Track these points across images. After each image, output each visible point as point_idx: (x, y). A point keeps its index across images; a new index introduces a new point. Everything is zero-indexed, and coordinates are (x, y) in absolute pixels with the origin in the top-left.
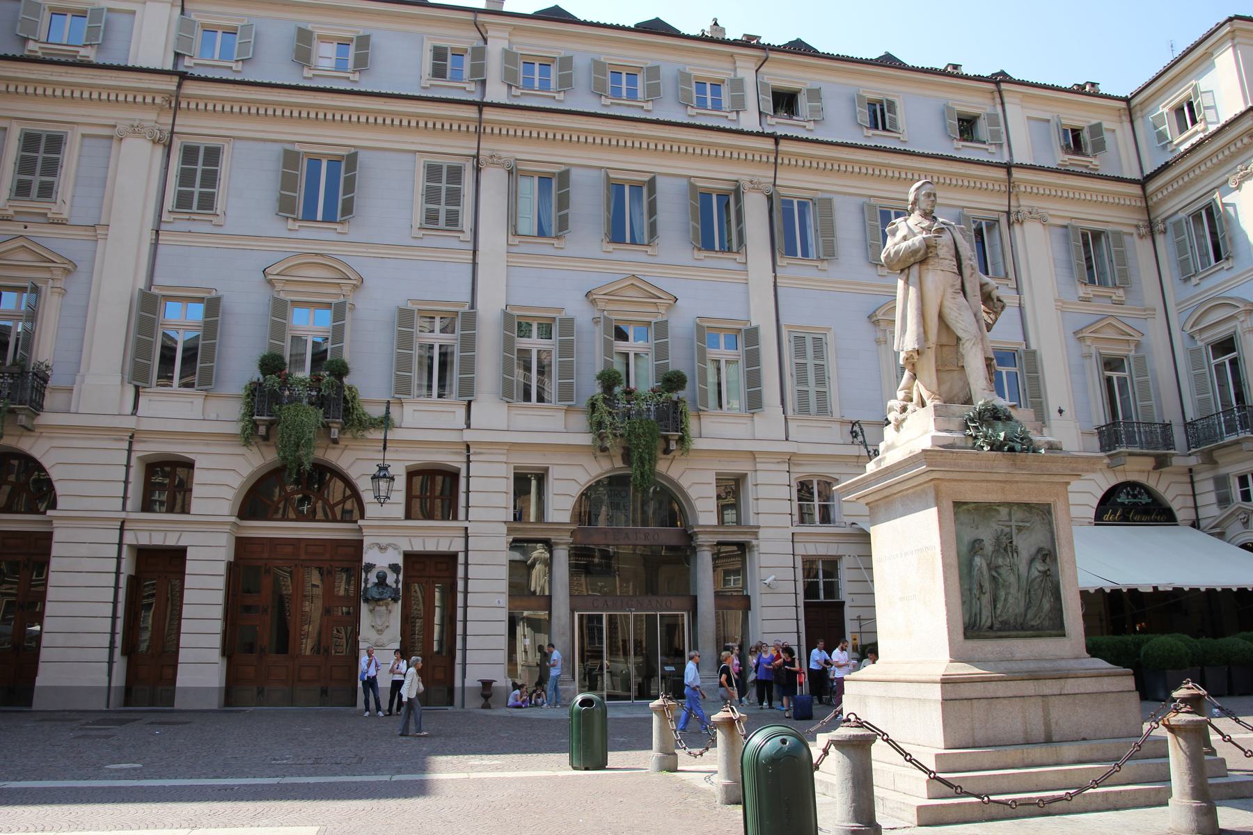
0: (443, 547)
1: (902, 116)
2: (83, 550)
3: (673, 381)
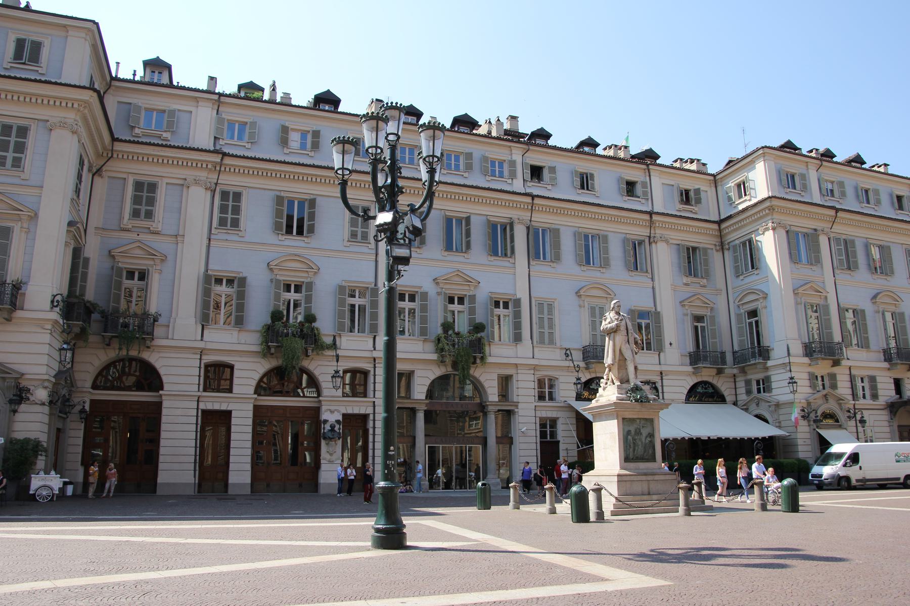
0: (363, 411)
1: (597, 182)
2: (179, 412)
3: (478, 328)
